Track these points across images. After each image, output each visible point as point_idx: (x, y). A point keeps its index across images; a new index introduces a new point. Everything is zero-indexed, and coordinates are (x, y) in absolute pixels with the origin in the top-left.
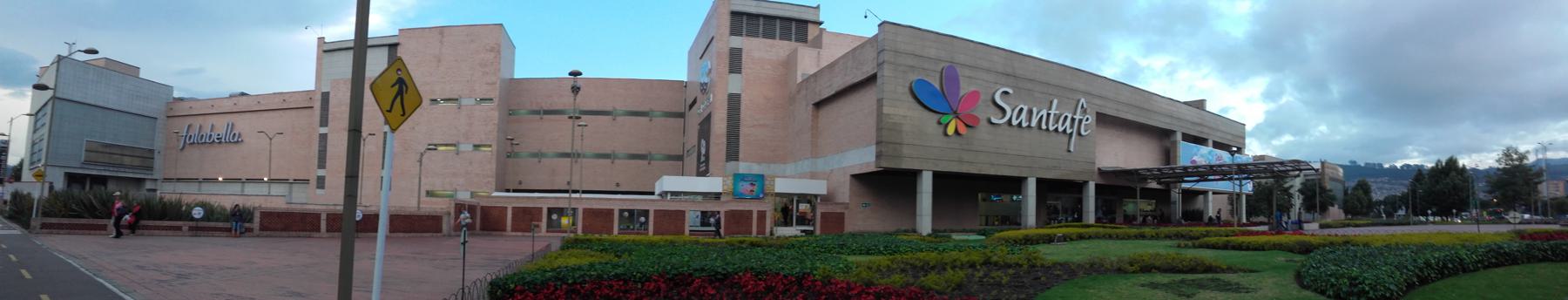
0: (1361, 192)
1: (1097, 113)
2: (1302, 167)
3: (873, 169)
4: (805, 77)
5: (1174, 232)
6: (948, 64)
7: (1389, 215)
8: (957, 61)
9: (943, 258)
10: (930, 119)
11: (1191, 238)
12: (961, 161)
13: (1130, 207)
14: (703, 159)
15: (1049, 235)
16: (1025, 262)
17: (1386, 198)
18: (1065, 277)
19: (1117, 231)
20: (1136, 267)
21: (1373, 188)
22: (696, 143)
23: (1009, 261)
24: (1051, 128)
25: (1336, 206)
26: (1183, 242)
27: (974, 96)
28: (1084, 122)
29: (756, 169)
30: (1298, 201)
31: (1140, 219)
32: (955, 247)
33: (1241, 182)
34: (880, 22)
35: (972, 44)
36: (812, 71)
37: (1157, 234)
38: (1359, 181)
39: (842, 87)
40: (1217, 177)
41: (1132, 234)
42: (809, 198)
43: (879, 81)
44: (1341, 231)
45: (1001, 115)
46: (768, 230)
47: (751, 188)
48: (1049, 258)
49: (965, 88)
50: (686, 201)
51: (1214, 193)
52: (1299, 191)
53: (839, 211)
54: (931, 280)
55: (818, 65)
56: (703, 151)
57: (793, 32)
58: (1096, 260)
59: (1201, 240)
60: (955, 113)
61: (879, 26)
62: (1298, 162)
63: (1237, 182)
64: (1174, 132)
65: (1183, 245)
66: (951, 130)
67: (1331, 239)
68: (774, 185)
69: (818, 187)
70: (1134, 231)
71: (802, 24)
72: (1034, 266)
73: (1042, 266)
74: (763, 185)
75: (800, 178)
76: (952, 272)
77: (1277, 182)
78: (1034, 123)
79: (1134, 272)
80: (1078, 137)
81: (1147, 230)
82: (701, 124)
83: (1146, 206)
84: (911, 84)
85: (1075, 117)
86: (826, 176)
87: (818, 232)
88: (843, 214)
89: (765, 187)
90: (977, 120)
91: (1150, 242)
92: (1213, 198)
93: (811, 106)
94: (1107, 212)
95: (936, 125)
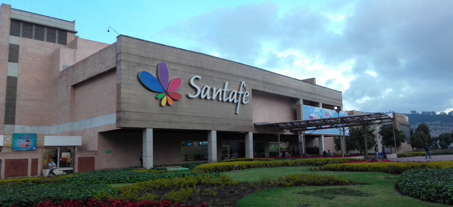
0: (422, 132)
1: (253, 90)
2: (382, 118)
3: (114, 128)
4: (66, 68)
6: (160, 62)
7: (444, 147)
9: (172, 182)
11: (317, 165)
12: (170, 122)
13: (273, 147)
15: (229, 166)
16: (222, 183)
17: (441, 136)
18: (249, 190)
19: (270, 162)
20: (291, 183)
21: (430, 129)
23: (212, 182)
24: (225, 100)
25: (406, 142)
26: (313, 168)
27: (177, 81)
28: (245, 96)
29: (28, 130)
30: (379, 140)
31: (281, 154)
32: (176, 175)
33: (344, 129)
34: (118, 35)
35: (175, 50)
36: (71, 64)
37: (295, 163)
38: (420, 125)
39: (92, 75)
41: (280, 164)
42: (69, 148)
44: (411, 159)
45: (194, 93)
46: (39, 172)
47: (27, 143)
48: (235, 180)
49: (171, 77)
51: (325, 136)
52: (379, 132)
54: (172, 195)
55: (74, 60)
58: (265, 180)
60: (166, 92)
61: (118, 37)
62: (380, 114)
63: (342, 129)
64: (299, 99)
65: (313, 169)
66: (164, 103)
67: (413, 164)
68: (43, 141)
69: (75, 141)
70: (280, 161)
71: (63, 32)
72: (227, 185)
73: (232, 185)
74: (36, 141)
75: (62, 135)
76: (184, 190)
77: (364, 128)
79: (290, 186)
80: (241, 105)
81: (289, 161)
83: (283, 146)
84: (138, 74)
85: (239, 93)
86: (81, 133)
87: (76, 170)
88: (94, 157)
89: (37, 142)
90: (180, 96)
91: (292, 168)
93: (70, 87)
94: (259, 151)
95: (154, 100)
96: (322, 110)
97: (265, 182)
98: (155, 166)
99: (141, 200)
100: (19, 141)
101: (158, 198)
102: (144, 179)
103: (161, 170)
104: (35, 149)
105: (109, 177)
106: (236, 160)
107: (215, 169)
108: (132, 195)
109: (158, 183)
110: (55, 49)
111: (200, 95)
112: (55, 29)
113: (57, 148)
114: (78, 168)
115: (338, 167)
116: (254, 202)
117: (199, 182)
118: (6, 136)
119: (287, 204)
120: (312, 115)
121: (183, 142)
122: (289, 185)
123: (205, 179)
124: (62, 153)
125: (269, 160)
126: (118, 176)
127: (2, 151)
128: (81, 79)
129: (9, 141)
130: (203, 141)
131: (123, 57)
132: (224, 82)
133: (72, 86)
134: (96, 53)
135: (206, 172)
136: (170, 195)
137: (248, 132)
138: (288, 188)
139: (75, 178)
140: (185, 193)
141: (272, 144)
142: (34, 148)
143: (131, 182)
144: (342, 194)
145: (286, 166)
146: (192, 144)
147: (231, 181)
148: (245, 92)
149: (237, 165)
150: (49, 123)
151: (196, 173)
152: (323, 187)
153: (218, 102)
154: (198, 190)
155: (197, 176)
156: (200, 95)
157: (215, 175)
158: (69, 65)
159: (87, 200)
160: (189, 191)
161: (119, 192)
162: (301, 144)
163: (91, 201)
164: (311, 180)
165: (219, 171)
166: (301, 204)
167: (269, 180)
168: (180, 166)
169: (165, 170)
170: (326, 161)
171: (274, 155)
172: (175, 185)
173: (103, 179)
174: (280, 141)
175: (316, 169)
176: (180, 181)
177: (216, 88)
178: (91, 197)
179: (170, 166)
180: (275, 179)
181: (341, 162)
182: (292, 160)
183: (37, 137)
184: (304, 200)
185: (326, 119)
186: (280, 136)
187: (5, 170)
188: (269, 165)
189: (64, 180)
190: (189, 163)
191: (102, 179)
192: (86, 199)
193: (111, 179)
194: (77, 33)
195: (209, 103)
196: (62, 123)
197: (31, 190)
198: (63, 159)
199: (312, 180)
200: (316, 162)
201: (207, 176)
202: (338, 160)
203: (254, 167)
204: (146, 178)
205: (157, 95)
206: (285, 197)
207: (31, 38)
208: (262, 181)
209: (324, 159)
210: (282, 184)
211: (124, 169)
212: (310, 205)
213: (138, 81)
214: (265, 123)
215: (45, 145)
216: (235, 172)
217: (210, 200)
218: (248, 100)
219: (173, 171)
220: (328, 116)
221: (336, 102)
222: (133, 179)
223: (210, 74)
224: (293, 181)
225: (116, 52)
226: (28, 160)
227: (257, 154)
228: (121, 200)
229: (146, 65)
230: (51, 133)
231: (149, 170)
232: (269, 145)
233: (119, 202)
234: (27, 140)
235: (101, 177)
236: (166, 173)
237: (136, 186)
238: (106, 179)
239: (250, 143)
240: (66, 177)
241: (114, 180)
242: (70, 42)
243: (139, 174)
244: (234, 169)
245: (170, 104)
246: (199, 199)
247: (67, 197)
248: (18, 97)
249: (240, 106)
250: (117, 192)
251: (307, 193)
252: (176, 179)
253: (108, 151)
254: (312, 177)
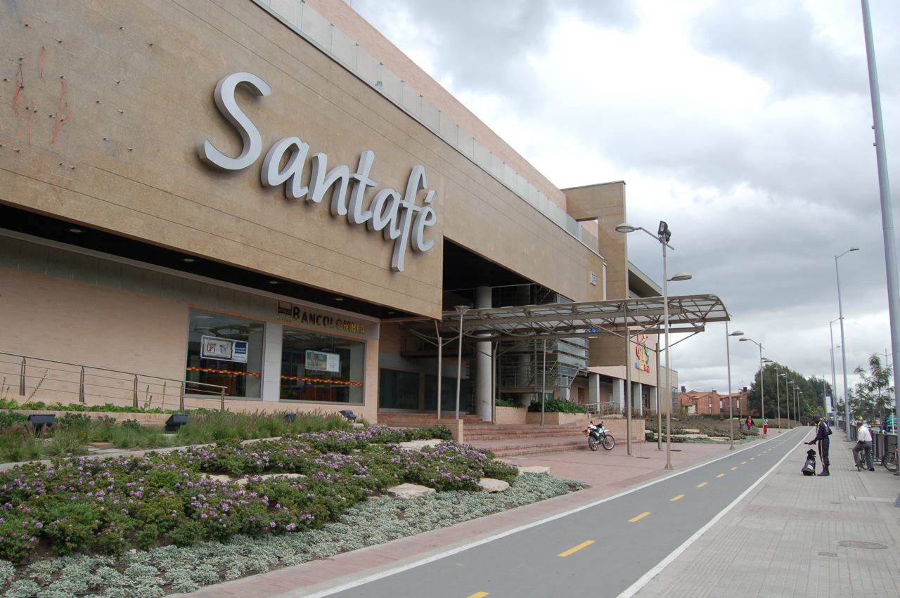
28: (422, 222)
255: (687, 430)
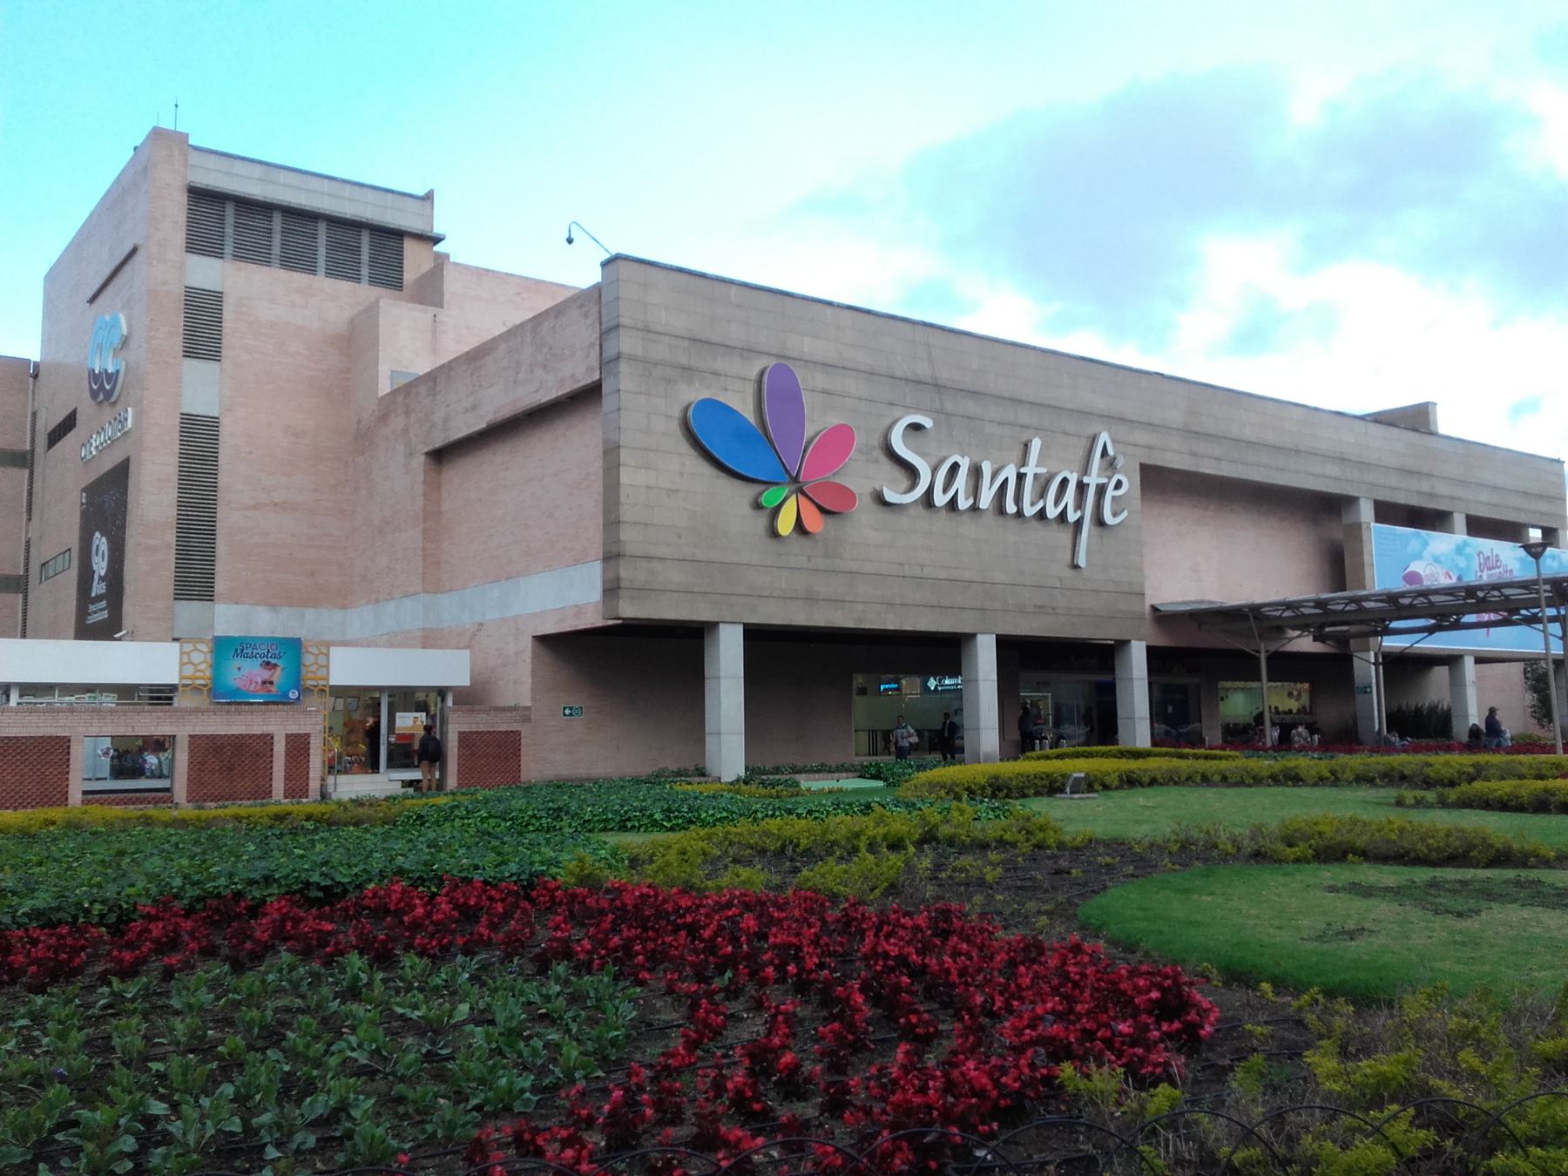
4: (401, 382)
5: (1381, 768)
6: (772, 362)
8: (794, 354)
10: (737, 496)
11: (1428, 783)
12: (810, 599)
14: (98, 588)
16: (1021, 837)
18: (1130, 869)
19: (1223, 764)
22: (73, 541)
23: (979, 835)
24: (1029, 511)
26: (1409, 795)
27: (840, 438)
28: (1110, 492)
29: (265, 623)
31: (1272, 734)
34: (606, 256)
35: (829, 310)
36: (422, 367)
37: (1333, 772)
39: (506, 413)
40: (1493, 617)
41: (1265, 773)
42: (420, 696)
43: (608, 402)
45: (905, 483)
46: (314, 785)
47: (266, 674)
48: (1070, 828)
49: (817, 422)
50: (71, 709)
51: (1480, 660)
53: (504, 728)
54: (826, 875)
55: (434, 351)
56: (100, 566)
57: (365, 256)
58: (1195, 834)
59: (1464, 787)
61: (605, 264)
65: (1410, 800)
66: (785, 524)
70: (1264, 764)
71: (390, 239)
72: (1040, 846)
73: (1061, 846)
75: (391, 645)
76: (871, 857)
78: (986, 499)
79: (1297, 860)
80: (1098, 530)
81: (1302, 763)
82: (93, 490)
83: (1283, 698)
84: (686, 409)
85: (1086, 480)
86: (469, 639)
88: (518, 733)
89: (303, 670)
90: (849, 496)
91: (1318, 792)
92: (1479, 678)
93: (422, 458)
95: (746, 509)
96: (1466, 544)
97: (1198, 840)
98: (753, 773)
99: (720, 888)
100: (238, 666)
101: (777, 885)
102: (719, 820)
103: (779, 788)
104: (298, 698)
105: (589, 809)
106: (1077, 752)
107: (990, 786)
108: (685, 872)
109: (774, 834)
110: (361, 308)
111: (929, 492)
112: (356, 226)
113: (377, 695)
114: (459, 773)
115: (1524, 793)
116: (1144, 909)
117: (926, 832)
118: (188, 647)
119: (1277, 923)
120: (1416, 567)
121: (860, 680)
122: (1292, 857)
123: (955, 821)
124: (398, 714)
125: (1221, 758)
126: (622, 806)
127: (176, 704)
128: (462, 428)
129: (203, 667)
130: (941, 673)
131: (627, 343)
132: (1025, 439)
133: (428, 454)
134: (522, 325)
135: (958, 798)
136: (823, 876)
137: (1128, 641)
138: (1291, 868)
139: (463, 809)
140: (875, 870)
141: (1235, 689)
142: (293, 695)
143: (671, 829)
144: (1514, 901)
145: (1290, 783)
146: (895, 686)
147: (1055, 832)
148: (1110, 478)
149: (1082, 775)
150: (341, 598)
151: (914, 800)
152: (1439, 869)
153: (1000, 520)
154: (926, 862)
155: (920, 813)
156: (929, 492)
157: (993, 810)
158: (411, 370)
159: (528, 884)
160: (891, 862)
161: (634, 862)
162: (1366, 692)
163: (546, 888)
164: (1388, 842)
165: (1007, 796)
166: (1335, 927)
167: (1213, 833)
168: (851, 774)
169: (791, 786)
170: (1471, 770)
171: (1242, 736)
172: (834, 843)
173: (567, 813)
174: (1270, 680)
175: (1423, 798)
176: (856, 829)
177: (992, 464)
178: (543, 873)
179: (811, 771)
180: (1237, 831)
181: (1544, 772)
182: (1320, 759)
183: (303, 650)
184: (1349, 915)
185: (1480, 588)
186: (1268, 659)
187: (190, 775)
188: (1217, 778)
189: (420, 817)
190: (886, 764)
191: (563, 814)
192: (527, 880)
193: (595, 816)
194: (443, 242)
195: (967, 527)
196: (392, 599)
197: (319, 847)
198: (400, 737)
199: (1394, 842)
200: (1427, 770)
201: (962, 812)
202: (1530, 767)
203: (1153, 782)
204: (725, 814)
205: (760, 494)
206: (1273, 897)
207: (268, 263)
208: (1182, 836)
209: (1465, 760)
210: (1266, 853)
211: (637, 781)
212: (1372, 931)
213: (683, 435)
214: (1201, 602)
215: (331, 683)
216: (1072, 799)
217: (975, 898)
218: (1123, 510)
219: (821, 792)
220: (1497, 571)
221: (1533, 505)
222: (676, 817)
223: (970, 407)
224: (1312, 841)
225: (601, 324)
226: (272, 738)
227: (1167, 733)
228: (650, 886)
229: (716, 374)
230: (349, 637)
231: (732, 783)
232: (1222, 694)
233: (645, 890)
234: (268, 663)
235: (556, 806)
236: (800, 799)
237: (692, 839)
238: (574, 816)
239: (1136, 684)
240: (427, 804)
241: (607, 820)
242: (416, 276)
243: (696, 798)
244: (1068, 790)
245: (810, 530)
246: (930, 891)
247: (460, 872)
248: (222, 496)
249: (1089, 537)
250: (626, 862)
251: (1367, 891)
252: (838, 820)
253: (571, 708)
254: (1392, 831)
255: (116, 811)
